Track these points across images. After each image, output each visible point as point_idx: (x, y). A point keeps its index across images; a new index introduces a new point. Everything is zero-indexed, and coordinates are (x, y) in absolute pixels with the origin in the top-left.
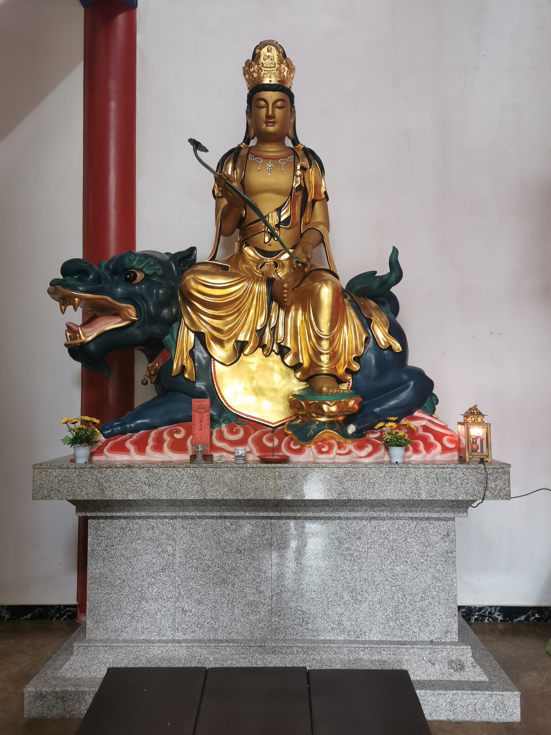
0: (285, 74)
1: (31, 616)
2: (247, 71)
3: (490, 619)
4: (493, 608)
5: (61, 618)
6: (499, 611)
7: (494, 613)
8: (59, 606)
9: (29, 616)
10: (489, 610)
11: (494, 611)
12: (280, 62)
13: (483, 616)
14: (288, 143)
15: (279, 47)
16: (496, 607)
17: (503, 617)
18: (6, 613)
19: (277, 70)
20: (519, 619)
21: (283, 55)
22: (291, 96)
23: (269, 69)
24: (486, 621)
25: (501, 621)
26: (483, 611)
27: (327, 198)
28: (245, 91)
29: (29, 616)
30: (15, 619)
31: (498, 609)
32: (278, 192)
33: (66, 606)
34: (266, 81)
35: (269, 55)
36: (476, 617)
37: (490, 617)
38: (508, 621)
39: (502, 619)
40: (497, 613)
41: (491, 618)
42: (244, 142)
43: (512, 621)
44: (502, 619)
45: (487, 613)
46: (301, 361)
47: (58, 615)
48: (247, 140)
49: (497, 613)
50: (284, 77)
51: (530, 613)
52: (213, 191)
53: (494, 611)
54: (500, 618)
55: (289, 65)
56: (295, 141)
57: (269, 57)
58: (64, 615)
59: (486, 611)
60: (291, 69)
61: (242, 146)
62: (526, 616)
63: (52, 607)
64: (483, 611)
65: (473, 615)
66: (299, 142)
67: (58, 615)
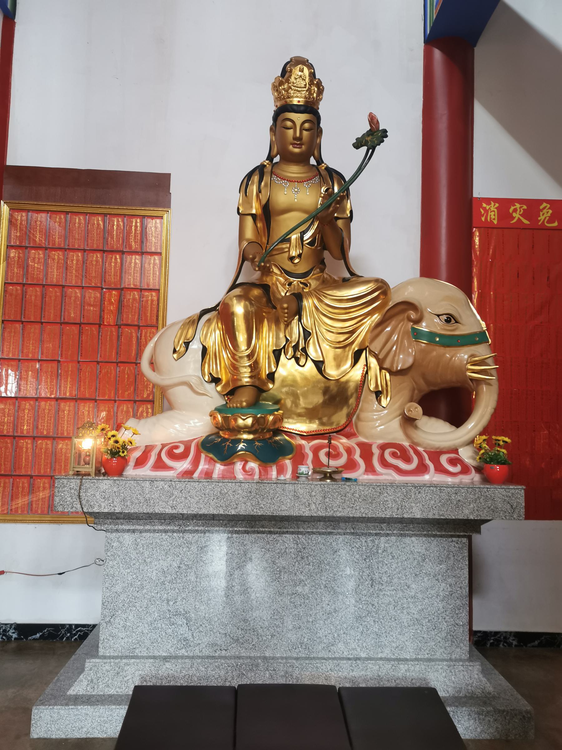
0: (315, 95)
1: (40, 636)
2: (276, 88)
3: (4, 637)
4: (9, 626)
5: (72, 638)
6: (15, 629)
7: (509, 638)
8: (70, 625)
9: (38, 635)
10: (4, 628)
11: (9, 629)
12: (311, 83)
13: (498, 641)
14: (313, 161)
15: (310, 66)
16: (511, 633)
17: (18, 634)
18: (13, 633)
19: (307, 91)
20: (34, 637)
21: (313, 75)
22: (318, 118)
23: (299, 89)
24: (501, 645)
25: (15, 639)
26: (499, 636)
27: (351, 218)
28: (271, 109)
29: (38, 635)
30: (22, 639)
31: (13, 627)
32: (305, 211)
33: (77, 626)
34: (295, 101)
35: (300, 76)
36: (492, 641)
37: (4, 635)
38: (22, 639)
39: (16, 636)
40: (12, 631)
41: (507, 643)
42: (267, 159)
43: (27, 639)
44: (16, 636)
45: (502, 637)
46: (380, 389)
47: (69, 634)
48: (270, 158)
49: (12, 631)
50: (313, 98)
51: (45, 631)
52: (238, 209)
53: (9, 629)
54: (515, 643)
55: (319, 85)
56: (320, 161)
57: (301, 76)
58: (75, 635)
59: (501, 636)
60: (321, 91)
61: (265, 164)
62: (41, 634)
63: (63, 626)
64: (499, 636)
65: (489, 640)
66: (323, 162)
67: (69, 634)
